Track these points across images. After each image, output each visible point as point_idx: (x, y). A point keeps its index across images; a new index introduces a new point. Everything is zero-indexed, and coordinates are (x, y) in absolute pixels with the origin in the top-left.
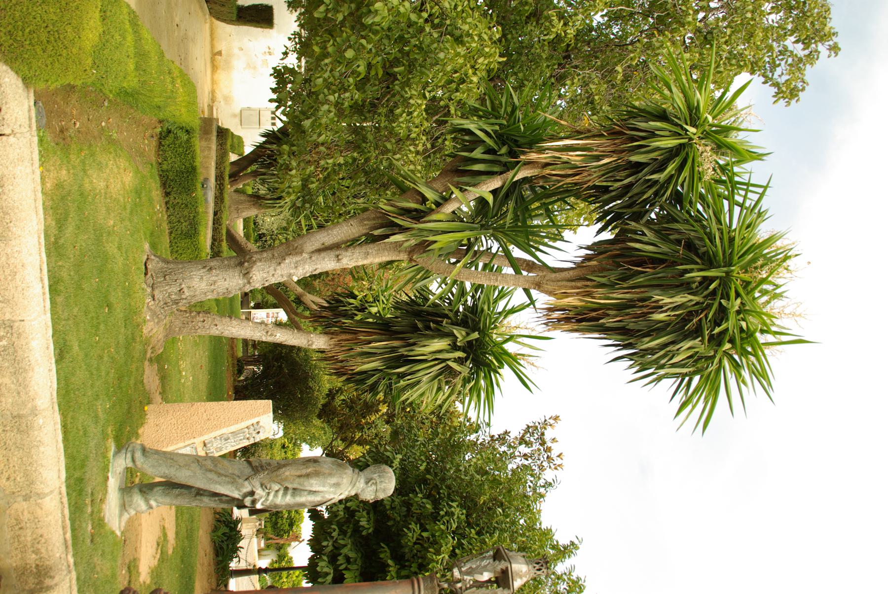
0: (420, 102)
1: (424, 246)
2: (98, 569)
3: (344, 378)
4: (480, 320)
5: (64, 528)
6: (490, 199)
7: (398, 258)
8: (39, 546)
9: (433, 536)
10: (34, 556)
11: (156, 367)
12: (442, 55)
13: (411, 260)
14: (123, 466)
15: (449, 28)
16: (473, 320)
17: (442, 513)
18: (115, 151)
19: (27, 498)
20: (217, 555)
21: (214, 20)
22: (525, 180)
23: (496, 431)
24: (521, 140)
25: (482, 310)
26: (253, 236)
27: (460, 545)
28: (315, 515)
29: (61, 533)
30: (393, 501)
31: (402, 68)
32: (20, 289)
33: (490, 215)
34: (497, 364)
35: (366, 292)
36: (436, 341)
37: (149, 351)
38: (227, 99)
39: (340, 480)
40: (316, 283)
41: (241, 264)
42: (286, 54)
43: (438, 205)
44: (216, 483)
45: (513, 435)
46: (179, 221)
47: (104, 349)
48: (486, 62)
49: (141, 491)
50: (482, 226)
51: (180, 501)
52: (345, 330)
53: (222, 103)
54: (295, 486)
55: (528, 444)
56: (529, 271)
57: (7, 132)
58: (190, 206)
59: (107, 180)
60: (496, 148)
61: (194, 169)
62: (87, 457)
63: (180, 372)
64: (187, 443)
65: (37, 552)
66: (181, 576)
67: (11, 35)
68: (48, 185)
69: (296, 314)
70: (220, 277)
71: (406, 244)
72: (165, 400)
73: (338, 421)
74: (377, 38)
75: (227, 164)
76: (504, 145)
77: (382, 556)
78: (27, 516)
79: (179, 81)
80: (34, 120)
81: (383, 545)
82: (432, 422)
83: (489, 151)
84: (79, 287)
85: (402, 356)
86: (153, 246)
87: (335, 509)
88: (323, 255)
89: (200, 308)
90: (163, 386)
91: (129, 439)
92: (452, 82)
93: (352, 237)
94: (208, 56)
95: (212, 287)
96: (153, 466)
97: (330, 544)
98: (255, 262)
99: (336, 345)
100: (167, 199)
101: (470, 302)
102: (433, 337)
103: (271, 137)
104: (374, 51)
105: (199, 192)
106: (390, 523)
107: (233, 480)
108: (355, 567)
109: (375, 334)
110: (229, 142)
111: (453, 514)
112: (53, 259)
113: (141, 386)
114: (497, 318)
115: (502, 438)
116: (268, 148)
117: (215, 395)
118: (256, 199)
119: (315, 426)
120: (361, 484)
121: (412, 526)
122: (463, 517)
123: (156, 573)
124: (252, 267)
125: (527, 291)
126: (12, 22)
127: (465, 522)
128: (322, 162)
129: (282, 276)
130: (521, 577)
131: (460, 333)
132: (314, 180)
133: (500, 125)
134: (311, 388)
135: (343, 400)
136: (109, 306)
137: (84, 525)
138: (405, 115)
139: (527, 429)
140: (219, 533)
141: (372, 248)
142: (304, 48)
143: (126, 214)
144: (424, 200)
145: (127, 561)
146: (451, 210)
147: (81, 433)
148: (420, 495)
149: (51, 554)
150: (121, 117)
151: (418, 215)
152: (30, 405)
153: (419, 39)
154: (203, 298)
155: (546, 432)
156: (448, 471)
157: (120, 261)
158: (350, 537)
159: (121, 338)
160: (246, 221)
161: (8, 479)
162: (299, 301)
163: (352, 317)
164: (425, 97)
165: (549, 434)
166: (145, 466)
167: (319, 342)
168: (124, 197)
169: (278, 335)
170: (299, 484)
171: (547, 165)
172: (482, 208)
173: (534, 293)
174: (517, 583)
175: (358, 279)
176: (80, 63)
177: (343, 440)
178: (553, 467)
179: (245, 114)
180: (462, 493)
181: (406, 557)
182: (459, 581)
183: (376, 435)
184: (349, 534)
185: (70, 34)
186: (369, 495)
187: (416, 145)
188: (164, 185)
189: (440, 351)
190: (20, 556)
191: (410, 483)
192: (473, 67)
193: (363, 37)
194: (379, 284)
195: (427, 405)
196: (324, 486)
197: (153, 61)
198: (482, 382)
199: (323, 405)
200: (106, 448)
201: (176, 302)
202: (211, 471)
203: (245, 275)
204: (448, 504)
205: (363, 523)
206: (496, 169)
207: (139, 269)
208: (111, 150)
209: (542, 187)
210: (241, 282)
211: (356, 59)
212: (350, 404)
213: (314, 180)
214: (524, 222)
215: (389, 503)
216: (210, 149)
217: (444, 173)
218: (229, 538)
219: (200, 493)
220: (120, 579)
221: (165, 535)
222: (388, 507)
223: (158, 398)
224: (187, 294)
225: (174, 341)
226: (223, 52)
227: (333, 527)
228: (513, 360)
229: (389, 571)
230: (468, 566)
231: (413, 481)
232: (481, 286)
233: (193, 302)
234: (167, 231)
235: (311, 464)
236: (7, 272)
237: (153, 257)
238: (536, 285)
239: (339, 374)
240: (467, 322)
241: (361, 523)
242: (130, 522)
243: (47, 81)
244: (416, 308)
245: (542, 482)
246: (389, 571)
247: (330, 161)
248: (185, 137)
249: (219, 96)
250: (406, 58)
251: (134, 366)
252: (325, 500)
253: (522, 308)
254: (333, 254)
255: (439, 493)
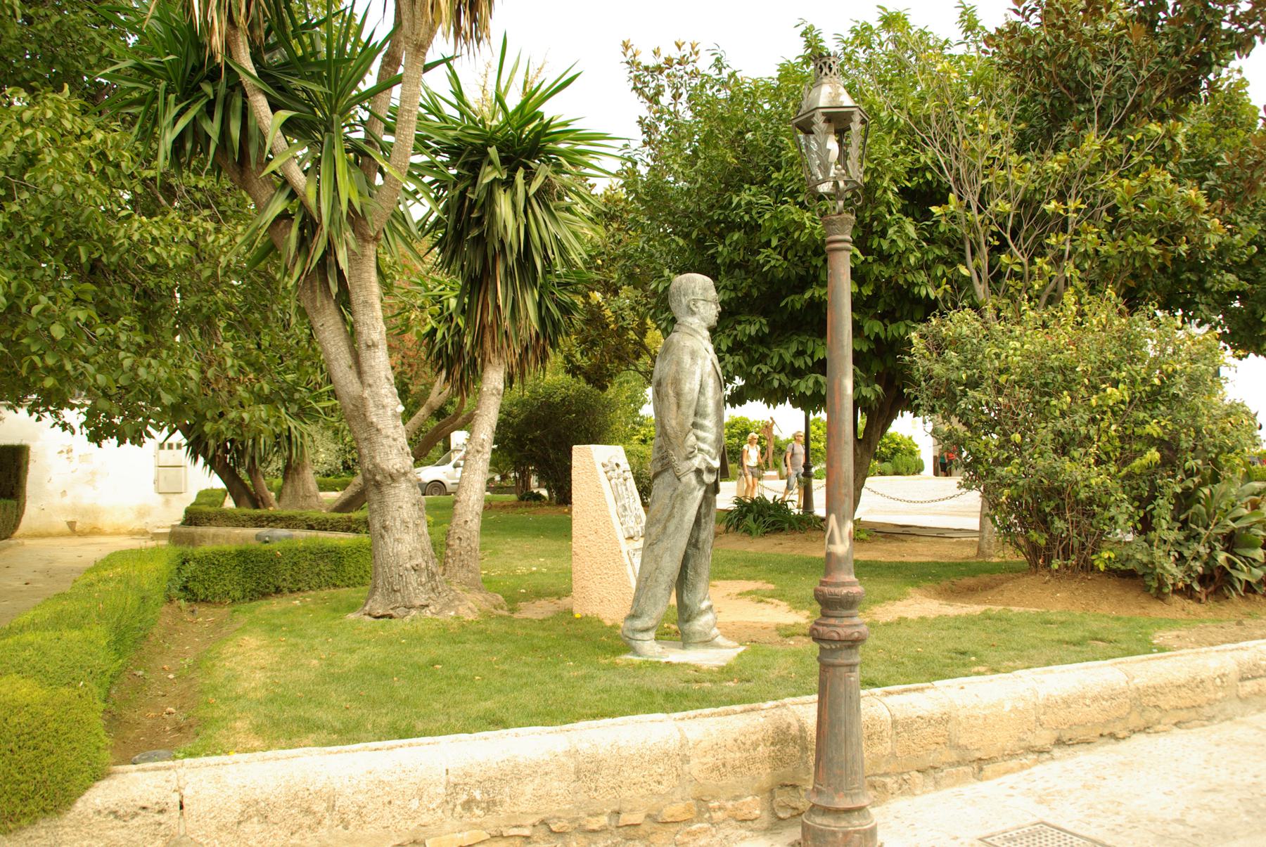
0: (136, 225)
1: (356, 219)
2: (784, 673)
3: (550, 351)
4: (471, 144)
5: (728, 714)
6: (284, 115)
7: (374, 259)
8: (749, 742)
9: (776, 232)
10: (760, 748)
11: (522, 604)
12: (58, 189)
13: (376, 239)
14: (653, 643)
15: (12, 173)
16: (471, 154)
17: (747, 218)
18: (211, 659)
19: (686, 760)
20: (783, 530)
21: (18, 533)
22: (256, 59)
23: (638, 137)
24: (193, 60)
25: (457, 140)
26: (345, 477)
27: (793, 194)
28: (737, 398)
29: (733, 717)
30: (725, 287)
31: (82, 250)
32: (403, 776)
33: (310, 117)
34: (537, 122)
35: (427, 315)
36: (498, 210)
37: (500, 612)
38: (142, 513)
39: (687, 350)
40: (414, 389)
41: (378, 485)
42: (65, 426)
43: (293, 195)
44: (681, 520)
45: (645, 113)
46: (318, 574)
47: (494, 670)
48: (69, 116)
49: (687, 621)
50: (327, 130)
51: (705, 573)
52: (479, 342)
53: (148, 520)
54: (691, 412)
55: (659, 92)
56: (399, 64)
57: (176, 798)
58: (295, 560)
59: (253, 669)
60: (204, 101)
61: (240, 553)
62: (638, 688)
63: (532, 573)
64: (627, 561)
65: (755, 745)
66: (805, 573)
67: (27, 798)
68: (256, 744)
69: (457, 415)
70: (396, 514)
71: (353, 245)
72: (568, 592)
73: (611, 362)
74: (31, 287)
75: (238, 511)
76: (200, 88)
77: (798, 306)
78: (709, 760)
79: (105, 573)
80: (159, 764)
81: (783, 304)
82: (619, 229)
83: (209, 111)
84: (405, 701)
85: (518, 260)
86: (352, 608)
87: (730, 368)
88: (365, 368)
89: (441, 548)
90: (551, 595)
91: (618, 637)
92: (103, 172)
93: (340, 325)
94: (77, 541)
95: (411, 525)
96: (655, 604)
97: (777, 376)
98: (375, 466)
99: (500, 356)
100: (286, 590)
101: (445, 158)
102: (493, 214)
103: (197, 447)
104: (52, 293)
105: (275, 546)
106: (755, 293)
107: (679, 498)
108: (810, 344)
109: (485, 299)
110: (206, 509)
111: (749, 203)
112: (363, 735)
113: (546, 623)
114: (470, 118)
115: (648, 129)
116: (215, 451)
117: (564, 530)
118: (291, 470)
119: (616, 396)
120: (694, 322)
121: (761, 258)
122: (754, 188)
123: (797, 604)
124: (383, 470)
125: (427, 68)
126: (5, 797)
127: (761, 186)
128: (231, 374)
129: (396, 427)
130: (838, 95)
131: (488, 175)
132: (257, 386)
133: (167, 92)
134: (563, 400)
135: (582, 353)
136: (433, 663)
137: (726, 690)
138: (157, 249)
139: (640, 92)
140: (754, 526)
141: (357, 297)
142: (53, 401)
143: (304, 644)
144: (284, 216)
145: (779, 639)
146: (302, 176)
147: (605, 696)
148: (720, 248)
149: (759, 728)
150: (161, 653)
151: (310, 225)
152: (564, 759)
153: (32, 222)
154: (426, 540)
155: (644, 64)
156: (687, 207)
157: (370, 650)
158: (770, 349)
159: (480, 647)
160: (323, 487)
161: (659, 783)
162: (439, 413)
163: (459, 332)
164: (129, 217)
165: (648, 60)
166: (654, 615)
167: (494, 378)
168: (279, 646)
169: (482, 436)
170: (689, 406)
171: (231, 20)
172: (300, 128)
173: (430, 58)
174: (846, 100)
175: (407, 326)
176: (69, 703)
177: (638, 357)
178: (694, 57)
179: (164, 488)
180: (720, 189)
181: (803, 273)
182: (836, 184)
183: (633, 309)
184: (766, 351)
185: (24, 718)
186: (710, 312)
187: (206, 232)
188: (265, 595)
189: (514, 205)
190: (758, 765)
191: (701, 262)
192: (78, 138)
193: (29, 309)
194: (414, 296)
195: (593, 234)
196: (694, 373)
197: (68, 605)
198: (562, 146)
199: (588, 382)
200: (628, 665)
201: (432, 576)
202: (665, 528)
203: (393, 480)
204: (735, 209)
205: (752, 330)
206: (238, 102)
207: (383, 626)
208: (209, 664)
209: (268, 34)
210: (404, 486)
211: (65, 322)
212: (588, 344)
213: (257, 386)
214: (320, 64)
215: (728, 293)
216: (215, 536)
217: (244, 184)
218: (760, 514)
219: (694, 543)
220: (800, 646)
221: (749, 593)
222: (733, 295)
223: (566, 601)
224: (420, 560)
225: (487, 581)
226: (70, 519)
227: (754, 370)
228: (533, 99)
229: (820, 297)
230: (816, 170)
231: (699, 258)
232: (420, 139)
233: (431, 552)
234: (332, 590)
235: (663, 390)
236: (379, 792)
237: (367, 608)
238: (418, 51)
239: (544, 357)
240: (474, 163)
241: (753, 333)
242: (728, 635)
243: (98, 748)
244: (449, 238)
245: (713, 73)
246: (820, 297)
247: (229, 362)
248: (192, 565)
249: (137, 525)
250: (65, 242)
251: (519, 631)
252: (713, 373)
253: (454, 78)
254: (365, 354)
255: (718, 222)
